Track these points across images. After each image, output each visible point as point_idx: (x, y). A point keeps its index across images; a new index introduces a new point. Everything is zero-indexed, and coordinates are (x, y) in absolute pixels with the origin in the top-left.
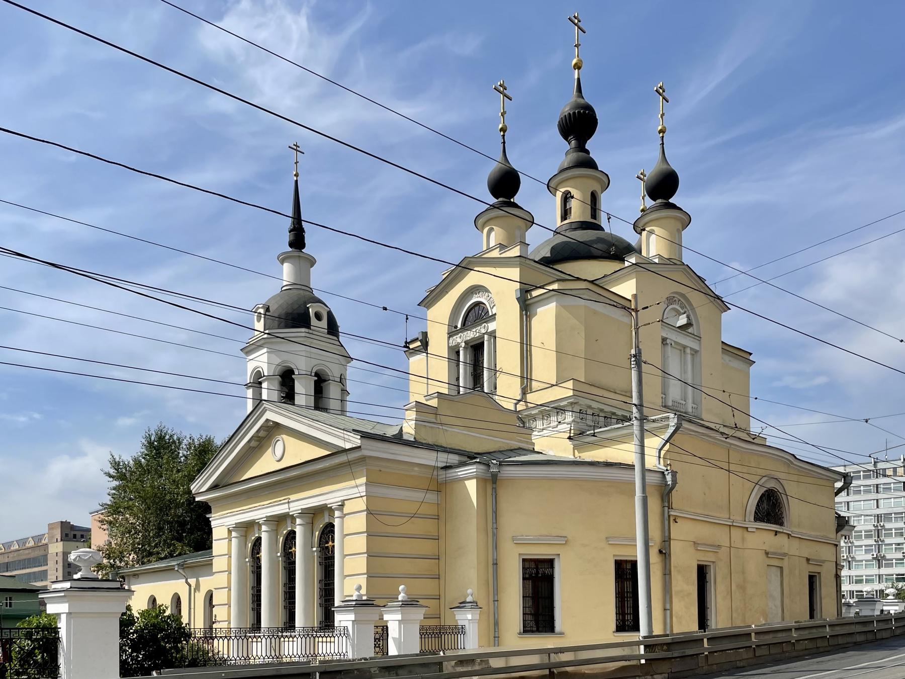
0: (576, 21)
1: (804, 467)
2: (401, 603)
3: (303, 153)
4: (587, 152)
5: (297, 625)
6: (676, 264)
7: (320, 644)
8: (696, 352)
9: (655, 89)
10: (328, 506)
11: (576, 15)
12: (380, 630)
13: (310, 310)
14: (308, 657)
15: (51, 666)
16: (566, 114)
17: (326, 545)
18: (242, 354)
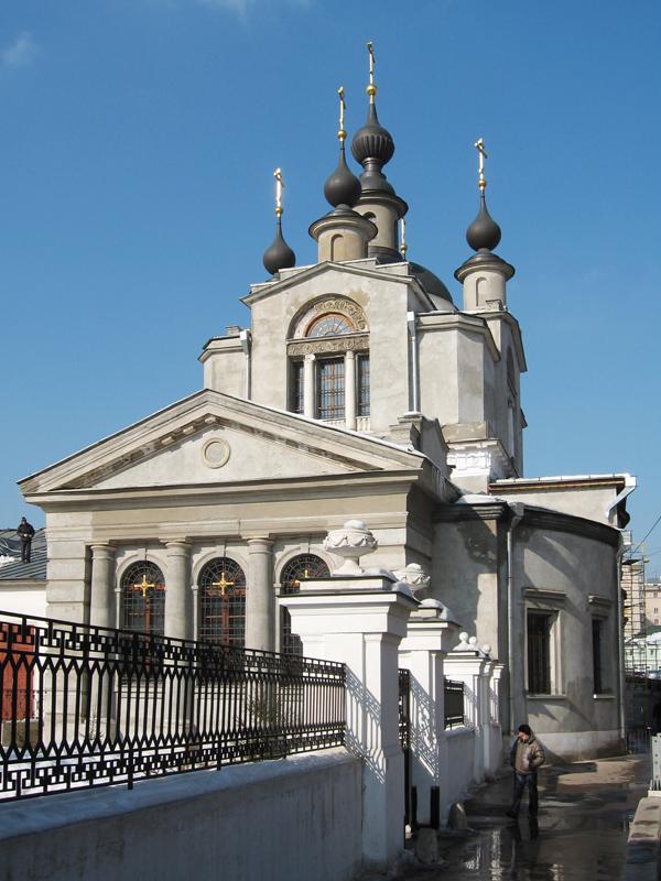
4: (384, 177)
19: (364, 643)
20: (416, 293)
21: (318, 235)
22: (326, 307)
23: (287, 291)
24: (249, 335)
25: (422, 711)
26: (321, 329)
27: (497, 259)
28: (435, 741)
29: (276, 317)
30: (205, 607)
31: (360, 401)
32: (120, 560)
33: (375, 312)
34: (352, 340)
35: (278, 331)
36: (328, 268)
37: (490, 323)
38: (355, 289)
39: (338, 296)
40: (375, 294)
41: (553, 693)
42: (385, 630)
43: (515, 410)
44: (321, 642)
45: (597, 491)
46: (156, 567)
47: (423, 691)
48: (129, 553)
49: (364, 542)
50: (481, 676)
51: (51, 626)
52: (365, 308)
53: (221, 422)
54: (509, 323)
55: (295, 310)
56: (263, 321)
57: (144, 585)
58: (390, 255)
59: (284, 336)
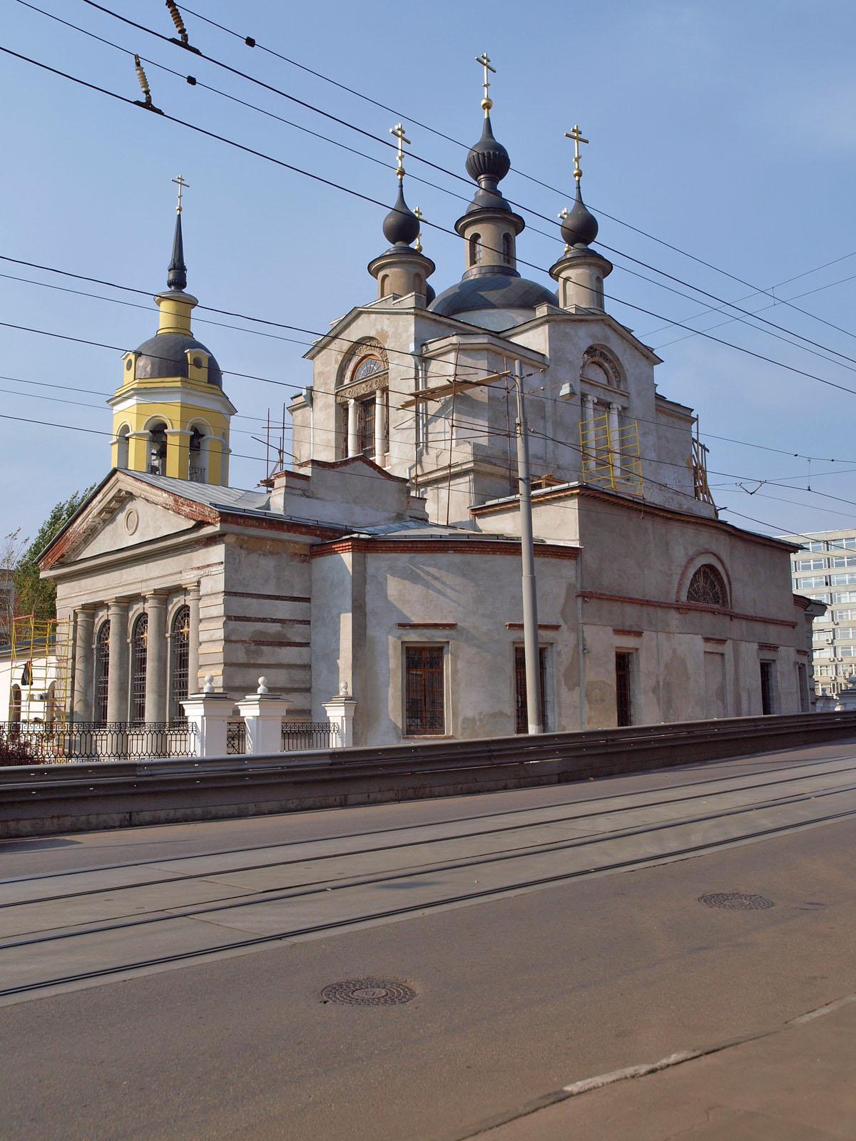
0: (485, 61)
2: (259, 696)
5: (109, 719)
6: (596, 314)
7: (173, 743)
8: (624, 409)
10: (183, 587)
11: (485, 56)
12: (234, 727)
13: (189, 355)
14: (140, 756)
17: (181, 631)
18: (108, 406)
22: (364, 351)
35: (329, 381)
40: (392, 330)
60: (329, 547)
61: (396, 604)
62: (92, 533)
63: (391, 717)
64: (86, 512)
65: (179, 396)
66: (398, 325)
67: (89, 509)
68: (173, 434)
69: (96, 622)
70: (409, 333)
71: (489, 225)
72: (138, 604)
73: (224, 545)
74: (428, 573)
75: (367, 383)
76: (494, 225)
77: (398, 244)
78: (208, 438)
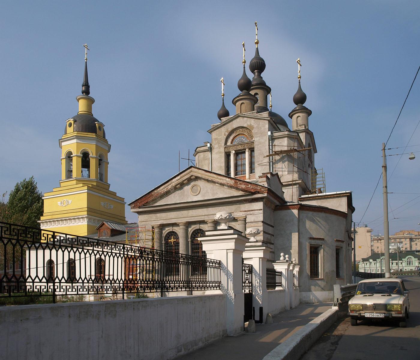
0: (86, 47)
1: (158, 208)
3: (89, 50)
4: (262, 78)
9: (297, 61)
10: (236, 218)
13: (97, 124)
15: (262, 359)
16: (253, 62)
19: (227, 253)
20: (272, 124)
21: (236, 103)
22: (238, 132)
23: (224, 126)
24: (211, 145)
25: (257, 280)
26: (236, 142)
27: (305, 108)
28: (261, 291)
29: (220, 137)
30: (193, 247)
31: (251, 168)
32: (164, 232)
33: (256, 133)
34: (248, 144)
35: (221, 142)
36: (239, 116)
37: (300, 135)
38: (249, 124)
39: (243, 127)
40: (256, 125)
41: (320, 277)
42: (234, 248)
43: (312, 168)
44: (212, 253)
45: (339, 199)
46: (176, 233)
47: (257, 273)
48: (167, 229)
49: (228, 217)
50: (288, 269)
51: (98, 241)
52: (253, 131)
53: (197, 178)
54: (309, 134)
55: (227, 134)
56: (216, 139)
57: (172, 240)
58: (264, 109)
59: (223, 144)
60: (287, 207)
61: (308, 230)
62: (167, 193)
63: (307, 271)
64: (168, 184)
65: (95, 141)
66: (260, 124)
67: (169, 183)
68: (92, 157)
69: (189, 231)
70: (265, 128)
71: (85, 100)
72: (196, 225)
73: (262, 202)
74: (318, 220)
75: (242, 145)
76: (263, 91)
77: (244, 91)
78: (105, 161)
